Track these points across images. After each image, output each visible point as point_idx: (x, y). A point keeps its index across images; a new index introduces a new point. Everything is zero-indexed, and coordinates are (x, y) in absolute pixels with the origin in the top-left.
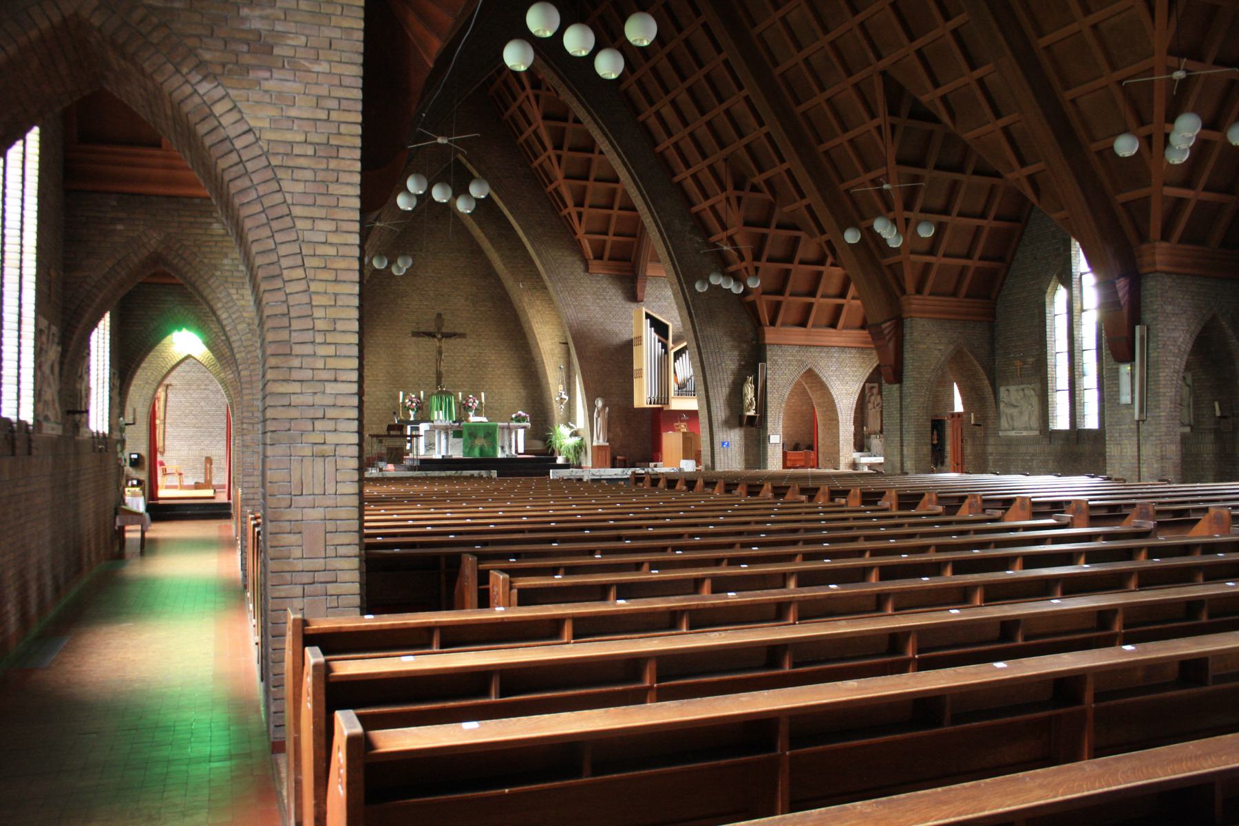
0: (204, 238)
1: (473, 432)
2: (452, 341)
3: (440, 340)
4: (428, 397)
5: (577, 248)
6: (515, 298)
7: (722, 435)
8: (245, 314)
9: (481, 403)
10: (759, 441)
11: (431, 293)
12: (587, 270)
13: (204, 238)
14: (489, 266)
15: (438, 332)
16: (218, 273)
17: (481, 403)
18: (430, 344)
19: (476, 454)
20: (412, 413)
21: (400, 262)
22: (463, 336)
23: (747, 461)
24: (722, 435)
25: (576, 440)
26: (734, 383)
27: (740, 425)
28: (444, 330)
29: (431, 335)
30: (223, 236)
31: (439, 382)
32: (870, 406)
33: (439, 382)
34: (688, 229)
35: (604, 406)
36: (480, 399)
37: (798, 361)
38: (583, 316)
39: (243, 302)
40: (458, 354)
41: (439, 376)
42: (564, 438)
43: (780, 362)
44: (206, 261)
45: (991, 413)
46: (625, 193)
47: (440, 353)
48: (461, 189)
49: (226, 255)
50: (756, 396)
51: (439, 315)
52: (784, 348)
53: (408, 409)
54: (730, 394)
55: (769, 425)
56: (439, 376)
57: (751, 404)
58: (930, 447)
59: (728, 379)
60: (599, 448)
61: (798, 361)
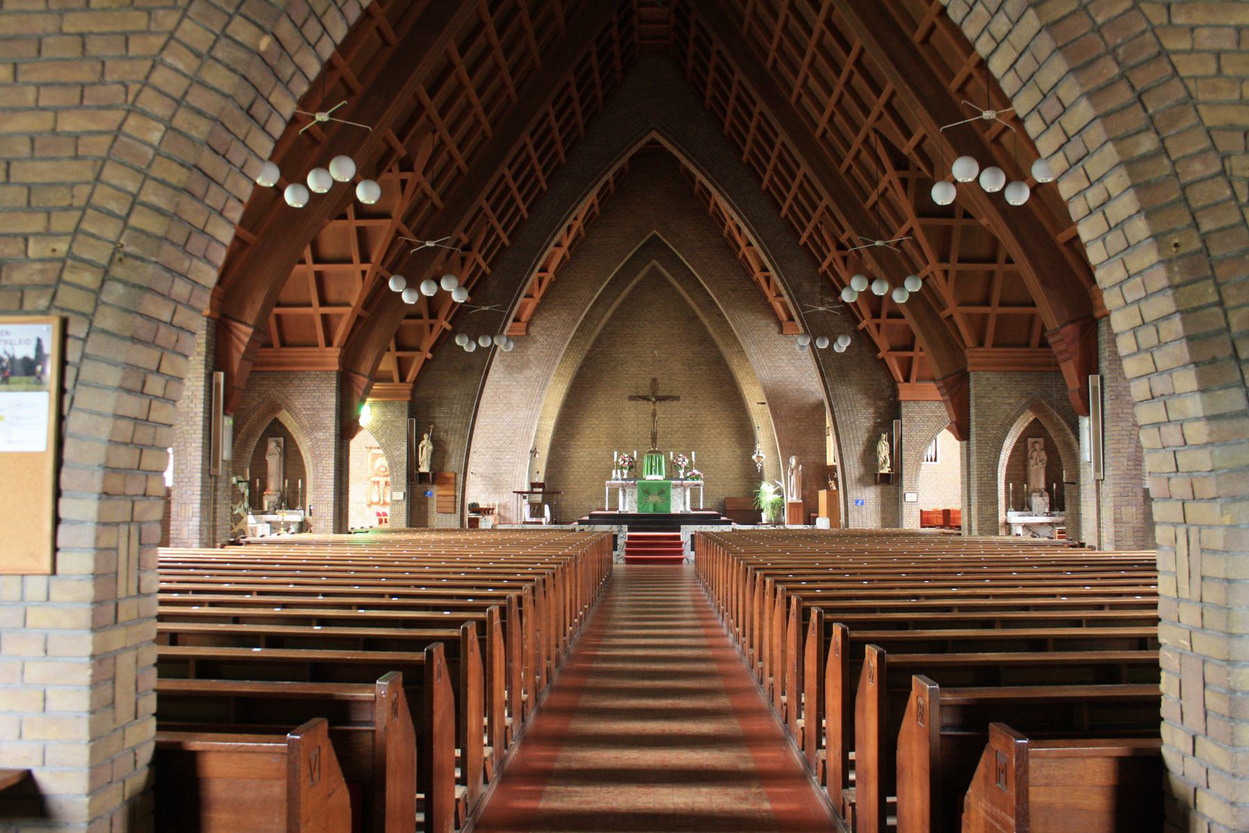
1: (646, 490)
2: (667, 403)
4: (640, 456)
5: (773, 313)
7: (856, 493)
9: (691, 462)
12: (781, 331)
14: (705, 332)
15: (655, 395)
17: (691, 462)
18: (649, 406)
19: (650, 510)
21: (840, 340)
22: (677, 398)
23: (883, 519)
24: (856, 493)
26: (868, 440)
27: (876, 483)
28: (660, 394)
32: (1032, 462)
35: (798, 464)
36: (690, 457)
37: (938, 417)
38: (778, 376)
40: (671, 416)
41: (654, 439)
42: (767, 494)
43: (917, 418)
46: (1016, 278)
47: (654, 415)
48: (897, 283)
51: (654, 380)
52: (921, 404)
54: (865, 451)
55: (905, 482)
56: (654, 439)
57: (885, 462)
58: (93, 552)
59: (863, 436)
60: (792, 505)
61: (938, 417)
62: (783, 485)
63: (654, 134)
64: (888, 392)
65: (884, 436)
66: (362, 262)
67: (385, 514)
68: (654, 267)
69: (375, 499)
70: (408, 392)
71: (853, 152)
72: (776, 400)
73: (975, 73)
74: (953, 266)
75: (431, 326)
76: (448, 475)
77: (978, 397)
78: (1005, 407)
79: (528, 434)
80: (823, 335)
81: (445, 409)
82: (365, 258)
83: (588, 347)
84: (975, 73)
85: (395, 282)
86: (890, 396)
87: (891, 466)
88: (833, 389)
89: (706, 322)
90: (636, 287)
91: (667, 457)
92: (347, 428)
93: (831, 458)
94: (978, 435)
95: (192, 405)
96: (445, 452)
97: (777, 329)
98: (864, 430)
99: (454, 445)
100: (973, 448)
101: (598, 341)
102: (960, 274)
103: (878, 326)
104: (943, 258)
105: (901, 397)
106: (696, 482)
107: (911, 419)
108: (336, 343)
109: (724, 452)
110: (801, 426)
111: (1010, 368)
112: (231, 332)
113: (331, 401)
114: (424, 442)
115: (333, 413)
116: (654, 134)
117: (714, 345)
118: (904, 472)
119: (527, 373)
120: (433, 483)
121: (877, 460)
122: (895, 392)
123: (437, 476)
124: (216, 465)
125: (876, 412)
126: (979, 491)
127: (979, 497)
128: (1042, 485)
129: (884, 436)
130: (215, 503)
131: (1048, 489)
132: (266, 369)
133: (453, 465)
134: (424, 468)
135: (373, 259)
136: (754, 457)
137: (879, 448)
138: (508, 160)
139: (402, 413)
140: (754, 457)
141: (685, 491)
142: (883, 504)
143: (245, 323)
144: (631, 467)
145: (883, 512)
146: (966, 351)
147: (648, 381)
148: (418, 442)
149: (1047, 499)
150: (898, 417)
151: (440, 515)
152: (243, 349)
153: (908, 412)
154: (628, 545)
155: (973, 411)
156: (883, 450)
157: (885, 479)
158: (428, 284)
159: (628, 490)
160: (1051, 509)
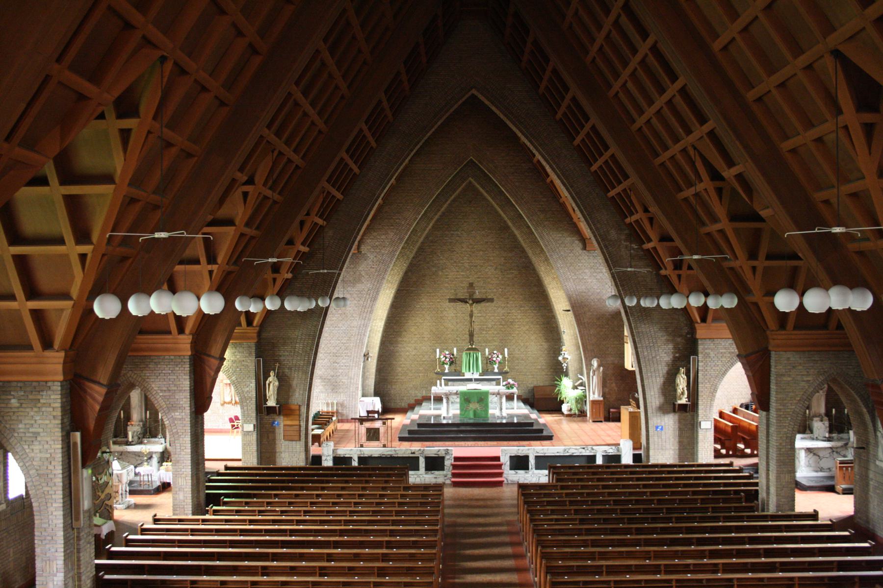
0: (7, 410)
3: (471, 305)
6: (536, 265)
7: (656, 420)
8: (35, 463)
9: (504, 357)
10: (693, 425)
11: (466, 265)
12: (584, 248)
13: (7, 410)
16: (16, 435)
17: (504, 357)
20: (447, 367)
22: (491, 300)
24: (656, 420)
25: (578, 392)
26: (668, 373)
27: (674, 411)
28: (477, 295)
29: (464, 301)
30: (18, 408)
31: (471, 341)
33: (471, 341)
34: (623, 237)
35: (599, 366)
36: (503, 354)
38: (581, 288)
39: (33, 455)
41: (471, 335)
43: (712, 354)
44: (8, 426)
45: (872, 440)
47: (471, 316)
49: (21, 422)
50: (688, 386)
51: (471, 285)
52: (717, 341)
53: (444, 363)
54: (664, 383)
55: (700, 412)
57: (683, 393)
59: (663, 369)
60: (594, 402)
62: (585, 379)
63: (474, 92)
64: (685, 330)
65: (682, 370)
66: (209, 263)
67: (237, 418)
68: (470, 182)
69: (228, 399)
70: (255, 335)
71: (638, 57)
72: (578, 308)
73: (760, 15)
74: (761, 263)
75: (275, 280)
76: (293, 407)
77: (779, 375)
78: (803, 384)
79: (362, 341)
80: (631, 294)
81: (288, 348)
82: (212, 259)
83: (412, 256)
84: (760, 15)
85: (241, 302)
86: (687, 333)
87: (688, 397)
88: (636, 328)
89: (516, 232)
90: (454, 201)
91: (483, 354)
92: (201, 401)
93: (629, 363)
94: (778, 410)
95: (51, 467)
96: (290, 386)
97: (581, 245)
98: (664, 364)
99: (297, 381)
100: (773, 420)
101: (421, 249)
102: (766, 269)
103: (679, 276)
104: (753, 255)
105: (698, 336)
106: (511, 391)
107: (707, 356)
108: (187, 331)
109: (532, 347)
110: (601, 333)
111: (809, 349)
112: (85, 392)
113: (185, 383)
114: (270, 379)
115: (188, 394)
116: (474, 92)
117: (523, 251)
118: (700, 402)
119: (360, 286)
120: (280, 414)
121: (675, 390)
122: (693, 331)
123: (284, 408)
124: (78, 519)
125: (675, 348)
126: (778, 461)
127: (779, 466)
128: (822, 410)
129: (682, 370)
130: (79, 552)
131: (828, 414)
132: (135, 354)
133: (297, 398)
134: (271, 403)
135: (219, 260)
136: (560, 358)
137: (678, 381)
138: (345, 147)
139: (250, 354)
140: (560, 358)
141: (501, 398)
142: (680, 429)
143: (99, 383)
144: (452, 363)
145: (680, 436)
146: (768, 332)
147: (466, 285)
148: (266, 379)
149: (827, 423)
150: (695, 352)
151: (287, 442)
152: (98, 407)
153: (704, 349)
154: (455, 467)
155: (773, 387)
156: (681, 382)
157: (683, 407)
158: (271, 299)
159: (451, 399)
160: (830, 432)
